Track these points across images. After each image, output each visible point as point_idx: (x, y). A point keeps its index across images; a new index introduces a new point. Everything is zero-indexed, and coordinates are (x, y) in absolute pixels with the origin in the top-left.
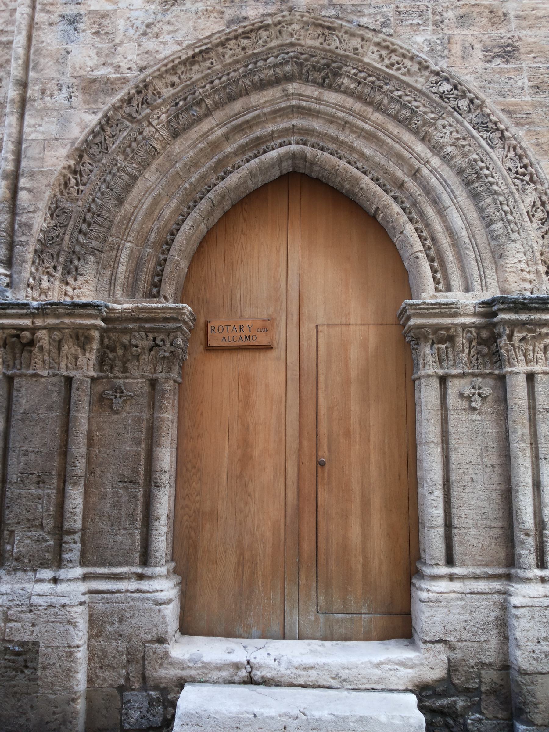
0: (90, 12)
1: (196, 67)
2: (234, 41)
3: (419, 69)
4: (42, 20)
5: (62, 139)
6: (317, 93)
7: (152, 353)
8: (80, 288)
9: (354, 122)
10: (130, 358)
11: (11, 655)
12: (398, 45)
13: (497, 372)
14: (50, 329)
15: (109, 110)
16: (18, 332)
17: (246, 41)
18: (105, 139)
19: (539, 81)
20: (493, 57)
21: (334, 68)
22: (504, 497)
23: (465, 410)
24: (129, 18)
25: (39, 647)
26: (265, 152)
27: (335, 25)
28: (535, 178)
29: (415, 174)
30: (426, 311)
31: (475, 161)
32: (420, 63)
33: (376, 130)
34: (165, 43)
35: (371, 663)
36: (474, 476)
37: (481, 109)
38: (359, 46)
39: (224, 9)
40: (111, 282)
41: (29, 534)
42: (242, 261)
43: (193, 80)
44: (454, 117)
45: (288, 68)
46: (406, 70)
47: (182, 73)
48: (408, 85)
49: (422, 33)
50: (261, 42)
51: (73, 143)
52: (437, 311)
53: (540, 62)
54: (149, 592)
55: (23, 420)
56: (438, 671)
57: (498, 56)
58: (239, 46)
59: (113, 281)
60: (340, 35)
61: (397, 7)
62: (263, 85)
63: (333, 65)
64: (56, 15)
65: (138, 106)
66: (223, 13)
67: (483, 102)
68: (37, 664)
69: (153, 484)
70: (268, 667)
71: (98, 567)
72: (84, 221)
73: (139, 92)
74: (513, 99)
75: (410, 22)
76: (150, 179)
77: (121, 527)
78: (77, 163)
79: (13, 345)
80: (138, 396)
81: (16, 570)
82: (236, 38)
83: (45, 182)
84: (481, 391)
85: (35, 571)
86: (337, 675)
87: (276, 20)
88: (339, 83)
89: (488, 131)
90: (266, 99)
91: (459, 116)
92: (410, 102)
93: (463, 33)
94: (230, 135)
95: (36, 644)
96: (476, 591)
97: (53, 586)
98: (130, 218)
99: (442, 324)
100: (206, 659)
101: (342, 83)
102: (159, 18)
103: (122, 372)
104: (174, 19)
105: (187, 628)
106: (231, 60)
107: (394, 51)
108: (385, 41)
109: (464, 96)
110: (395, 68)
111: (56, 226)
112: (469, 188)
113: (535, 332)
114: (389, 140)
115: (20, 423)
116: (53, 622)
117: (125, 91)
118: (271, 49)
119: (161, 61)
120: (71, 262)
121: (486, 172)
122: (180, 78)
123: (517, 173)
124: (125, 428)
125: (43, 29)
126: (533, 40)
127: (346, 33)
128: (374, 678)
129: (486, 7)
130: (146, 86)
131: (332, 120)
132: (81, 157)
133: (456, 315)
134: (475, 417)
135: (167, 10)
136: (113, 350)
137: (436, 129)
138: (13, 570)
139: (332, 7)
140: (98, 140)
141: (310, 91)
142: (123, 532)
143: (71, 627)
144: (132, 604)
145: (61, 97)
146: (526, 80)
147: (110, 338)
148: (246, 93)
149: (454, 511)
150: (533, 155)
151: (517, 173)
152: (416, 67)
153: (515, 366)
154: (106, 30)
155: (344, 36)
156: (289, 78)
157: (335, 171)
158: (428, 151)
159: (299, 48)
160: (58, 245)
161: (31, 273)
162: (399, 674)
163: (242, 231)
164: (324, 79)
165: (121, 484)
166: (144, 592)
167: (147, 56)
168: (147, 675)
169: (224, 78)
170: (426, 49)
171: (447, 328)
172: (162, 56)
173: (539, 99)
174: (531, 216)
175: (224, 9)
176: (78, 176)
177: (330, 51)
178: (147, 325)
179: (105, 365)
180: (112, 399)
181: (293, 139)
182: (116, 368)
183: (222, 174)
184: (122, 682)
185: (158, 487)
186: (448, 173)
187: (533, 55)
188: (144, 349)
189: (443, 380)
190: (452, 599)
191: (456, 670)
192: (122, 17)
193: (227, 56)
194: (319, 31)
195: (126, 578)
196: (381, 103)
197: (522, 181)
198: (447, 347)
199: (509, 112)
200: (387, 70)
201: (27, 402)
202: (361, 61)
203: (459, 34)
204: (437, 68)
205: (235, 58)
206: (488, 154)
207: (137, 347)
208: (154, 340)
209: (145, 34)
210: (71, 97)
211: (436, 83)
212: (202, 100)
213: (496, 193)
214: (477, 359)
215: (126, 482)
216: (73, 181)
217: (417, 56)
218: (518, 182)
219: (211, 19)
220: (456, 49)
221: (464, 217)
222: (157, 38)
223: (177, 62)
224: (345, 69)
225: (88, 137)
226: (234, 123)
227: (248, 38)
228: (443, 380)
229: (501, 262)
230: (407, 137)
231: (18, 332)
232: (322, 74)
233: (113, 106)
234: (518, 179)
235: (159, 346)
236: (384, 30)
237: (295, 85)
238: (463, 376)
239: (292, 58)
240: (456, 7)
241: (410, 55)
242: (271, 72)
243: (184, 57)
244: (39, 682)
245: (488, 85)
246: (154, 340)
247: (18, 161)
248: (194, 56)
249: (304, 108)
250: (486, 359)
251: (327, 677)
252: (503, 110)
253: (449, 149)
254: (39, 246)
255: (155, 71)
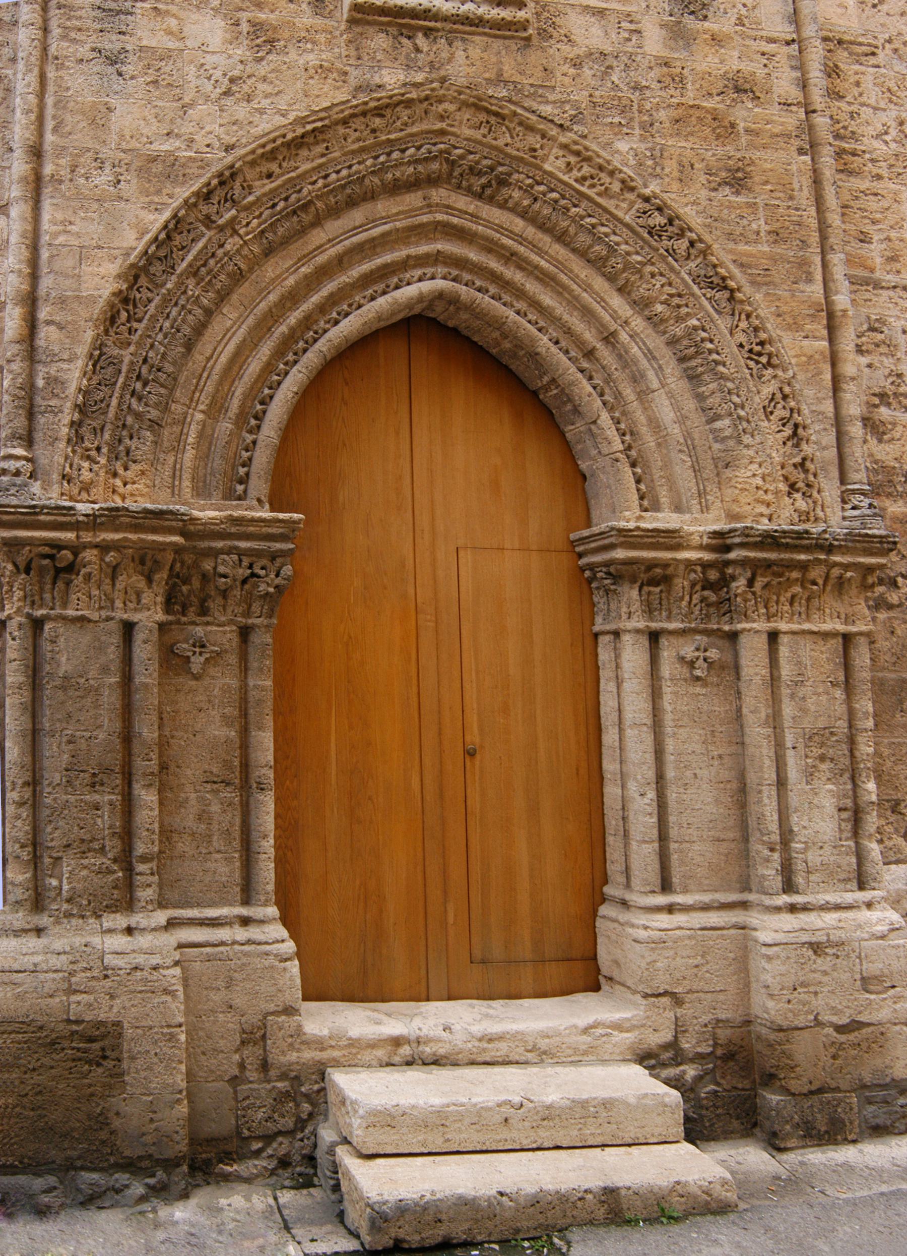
0: (142, 49)
1: (304, 153)
2: (362, 119)
3: (621, 190)
4: (65, 53)
5: (109, 248)
6: (472, 206)
7: (247, 587)
8: (134, 483)
9: (526, 255)
10: (213, 593)
11: (81, 1041)
12: (593, 151)
13: (726, 628)
14: (104, 548)
15: (179, 209)
16: (54, 551)
17: (378, 121)
18: (172, 252)
19: (779, 225)
20: (719, 185)
21: (502, 173)
22: (735, 798)
23: (685, 680)
24: (202, 65)
25: (122, 1028)
26: (397, 287)
27: (506, 112)
28: (775, 361)
29: (610, 339)
30: (639, 540)
31: (695, 328)
32: (623, 182)
33: (556, 270)
34: (261, 111)
35: (575, 1026)
36: (698, 771)
37: (705, 256)
38: (538, 146)
39: (348, 68)
40: (174, 474)
41: (85, 862)
42: (345, 445)
43: (299, 171)
44: (667, 264)
45: (435, 166)
46: (603, 188)
47: (284, 159)
48: (605, 210)
49: (626, 137)
50: (398, 123)
51: (128, 255)
52: (653, 540)
53: (779, 198)
54: (266, 943)
55: (64, 688)
56: (662, 1034)
57: (726, 183)
58: (367, 126)
59: (178, 473)
60: (512, 126)
61: (591, 96)
62: (396, 188)
63: (500, 169)
64: (88, 47)
65: (219, 203)
66: (346, 73)
67: (709, 247)
68: (121, 1052)
69: (255, 785)
70: (439, 1040)
71: (182, 908)
72: (139, 377)
73: (222, 183)
74: (746, 247)
75: (609, 120)
76: (231, 316)
77: (212, 849)
78: (130, 288)
79: (42, 571)
80: (226, 651)
81: (69, 915)
82: (364, 114)
83: (85, 314)
84: (708, 654)
85: (99, 917)
86: (534, 1046)
87: (423, 95)
88: (506, 196)
89: (713, 289)
90: (401, 208)
91: (675, 264)
92: (607, 235)
93: (680, 144)
94: (345, 259)
95: (118, 1024)
96: (708, 925)
97: (129, 938)
98: (201, 375)
99: (661, 559)
100: (354, 1033)
101: (510, 197)
102: (249, 70)
103: (199, 615)
104: (273, 75)
105: (315, 992)
106: (355, 146)
107: (588, 159)
108: (576, 143)
109: (681, 235)
110: (587, 183)
111: (99, 384)
112: (684, 366)
113: (781, 575)
114: (575, 287)
115: (60, 693)
116: (140, 992)
117: (203, 180)
118: (412, 135)
119: (257, 138)
120: (120, 441)
121: (709, 346)
122: (280, 166)
123: (751, 351)
124: (210, 702)
125: (68, 68)
126: (769, 166)
127: (521, 124)
128: (584, 1047)
129: (707, 111)
130: (233, 176)
131: (491, 247)
132: (136, 277)
133: (678, 547)
134: (698, 690)
135: (262, 59)
136: (186, 581)
137: (641, 277)
138: (65, 917)
139: (502, 84)
140: (162, 253)
141: (462, 202)
142: (218, 856)
143: (169, 998)
144: (244, 960)
145: (103, 179)
146: (762, 222)
147: (183, 563)
148: (371, 196)
149: (672, 819)
150: (773, 328)
151: (751, 351)
152: (616, 187)
153: (754, 621)
154: (169, 80)
155: (518, 129)
156: (433, 181)
157: (498, 324)
158: (628, 307)
159: (452, 138)
160: (103, 414)
161: (67, 457)
162: (614, 1040)
163: (343, 399)
164: (483, 187)
165: (209, 786)
166: (259, 944)
167: (235, 128)
168: (270, 1060)
169: (344, 173)
170: (632, 162)
171: (666, 565)
172: (259, 131)
173: (779, 251)
174: (768, 414)
175: (348, 68)
176: (131, 307)
177: (496, 148)
178: (243, 544)
179: (175, 603)
180: (188, 657)
181: (441, 270)
182: (192, 609)
183: (334, 315)
184: (236, 1072)
185: (262, 789)
186: (656, 342)
187: (769, 187)
188: (235, 580)
189: (654, 637)
190: (680, 938)
191: (684, 1031)
192: (192, 62)
193: (349, 140)
194: (483, 117)
195: (226, 923)
196: (565, 232)
197: (757, 362)
198: (661, 591)
199: (742, 265)
200: (577, 186)
201: (68, 659)
202: (540, 168)
203: (679, 146)
204: (647, 192)
205: (361, 144)
206: (712, 321)
207: (225, 576)
208: (251, 567)
209: (227, 93)
210: (119, 182)
211: (645, 213)
212: (310, 202)
213: (722, 377)
214: (701, 610)
215: (215, 782)
216: (124, 315)
217: (621, 171)
218: (752, 364)
219: (330, 81)
220: (671, 167)
221: (676, 407)
222: (248, 101)
223: (279, 142)
224: (516, 176)
225: (149, 247)
226: (354, 240)
227: (383, 116)
228: (654, 637)
229: (728, 473)
230: (599, 283)
231: (54, 551)
232: (483, 180)
233: (186, 201)
234: (752, 359)
235: (259, 577)
236: (575, 128)
237: (443, 192)
238: (683, 632)
239: (441, 152)
240: (669, 106)
241: (610, 168)
242: (411, 169)
243: (290, 136)
244: (126, 1078)
245: (715, 224)
246: (251, 567)
247: (34, 277)
248: (303, 136)
249: (454, 227)
250: (712, 610)
251: (521, 1050)
252: (734, 261)
253: (659, 308)
254: (77, 416)
255: (247, 154)
